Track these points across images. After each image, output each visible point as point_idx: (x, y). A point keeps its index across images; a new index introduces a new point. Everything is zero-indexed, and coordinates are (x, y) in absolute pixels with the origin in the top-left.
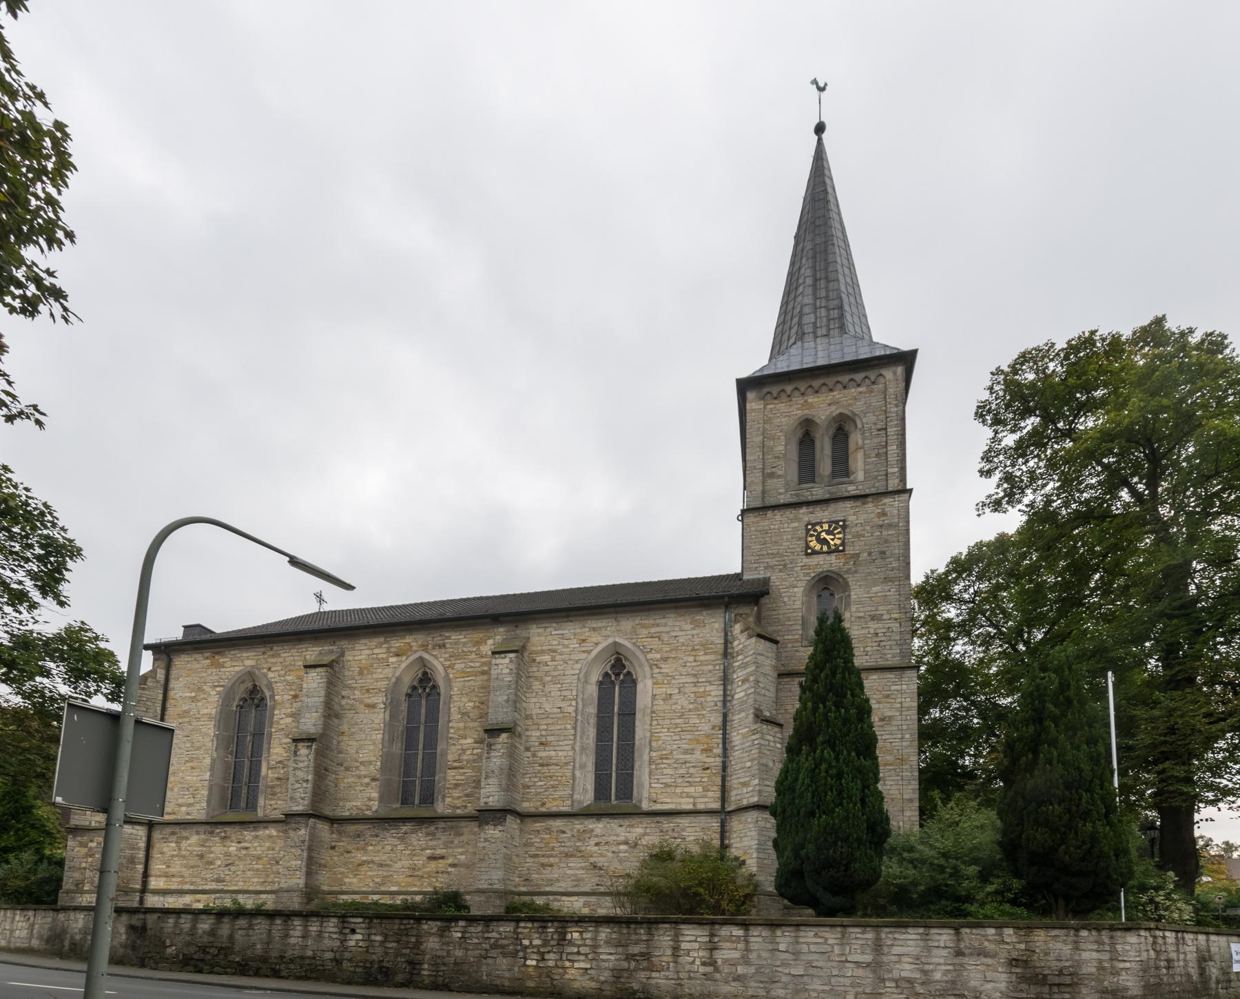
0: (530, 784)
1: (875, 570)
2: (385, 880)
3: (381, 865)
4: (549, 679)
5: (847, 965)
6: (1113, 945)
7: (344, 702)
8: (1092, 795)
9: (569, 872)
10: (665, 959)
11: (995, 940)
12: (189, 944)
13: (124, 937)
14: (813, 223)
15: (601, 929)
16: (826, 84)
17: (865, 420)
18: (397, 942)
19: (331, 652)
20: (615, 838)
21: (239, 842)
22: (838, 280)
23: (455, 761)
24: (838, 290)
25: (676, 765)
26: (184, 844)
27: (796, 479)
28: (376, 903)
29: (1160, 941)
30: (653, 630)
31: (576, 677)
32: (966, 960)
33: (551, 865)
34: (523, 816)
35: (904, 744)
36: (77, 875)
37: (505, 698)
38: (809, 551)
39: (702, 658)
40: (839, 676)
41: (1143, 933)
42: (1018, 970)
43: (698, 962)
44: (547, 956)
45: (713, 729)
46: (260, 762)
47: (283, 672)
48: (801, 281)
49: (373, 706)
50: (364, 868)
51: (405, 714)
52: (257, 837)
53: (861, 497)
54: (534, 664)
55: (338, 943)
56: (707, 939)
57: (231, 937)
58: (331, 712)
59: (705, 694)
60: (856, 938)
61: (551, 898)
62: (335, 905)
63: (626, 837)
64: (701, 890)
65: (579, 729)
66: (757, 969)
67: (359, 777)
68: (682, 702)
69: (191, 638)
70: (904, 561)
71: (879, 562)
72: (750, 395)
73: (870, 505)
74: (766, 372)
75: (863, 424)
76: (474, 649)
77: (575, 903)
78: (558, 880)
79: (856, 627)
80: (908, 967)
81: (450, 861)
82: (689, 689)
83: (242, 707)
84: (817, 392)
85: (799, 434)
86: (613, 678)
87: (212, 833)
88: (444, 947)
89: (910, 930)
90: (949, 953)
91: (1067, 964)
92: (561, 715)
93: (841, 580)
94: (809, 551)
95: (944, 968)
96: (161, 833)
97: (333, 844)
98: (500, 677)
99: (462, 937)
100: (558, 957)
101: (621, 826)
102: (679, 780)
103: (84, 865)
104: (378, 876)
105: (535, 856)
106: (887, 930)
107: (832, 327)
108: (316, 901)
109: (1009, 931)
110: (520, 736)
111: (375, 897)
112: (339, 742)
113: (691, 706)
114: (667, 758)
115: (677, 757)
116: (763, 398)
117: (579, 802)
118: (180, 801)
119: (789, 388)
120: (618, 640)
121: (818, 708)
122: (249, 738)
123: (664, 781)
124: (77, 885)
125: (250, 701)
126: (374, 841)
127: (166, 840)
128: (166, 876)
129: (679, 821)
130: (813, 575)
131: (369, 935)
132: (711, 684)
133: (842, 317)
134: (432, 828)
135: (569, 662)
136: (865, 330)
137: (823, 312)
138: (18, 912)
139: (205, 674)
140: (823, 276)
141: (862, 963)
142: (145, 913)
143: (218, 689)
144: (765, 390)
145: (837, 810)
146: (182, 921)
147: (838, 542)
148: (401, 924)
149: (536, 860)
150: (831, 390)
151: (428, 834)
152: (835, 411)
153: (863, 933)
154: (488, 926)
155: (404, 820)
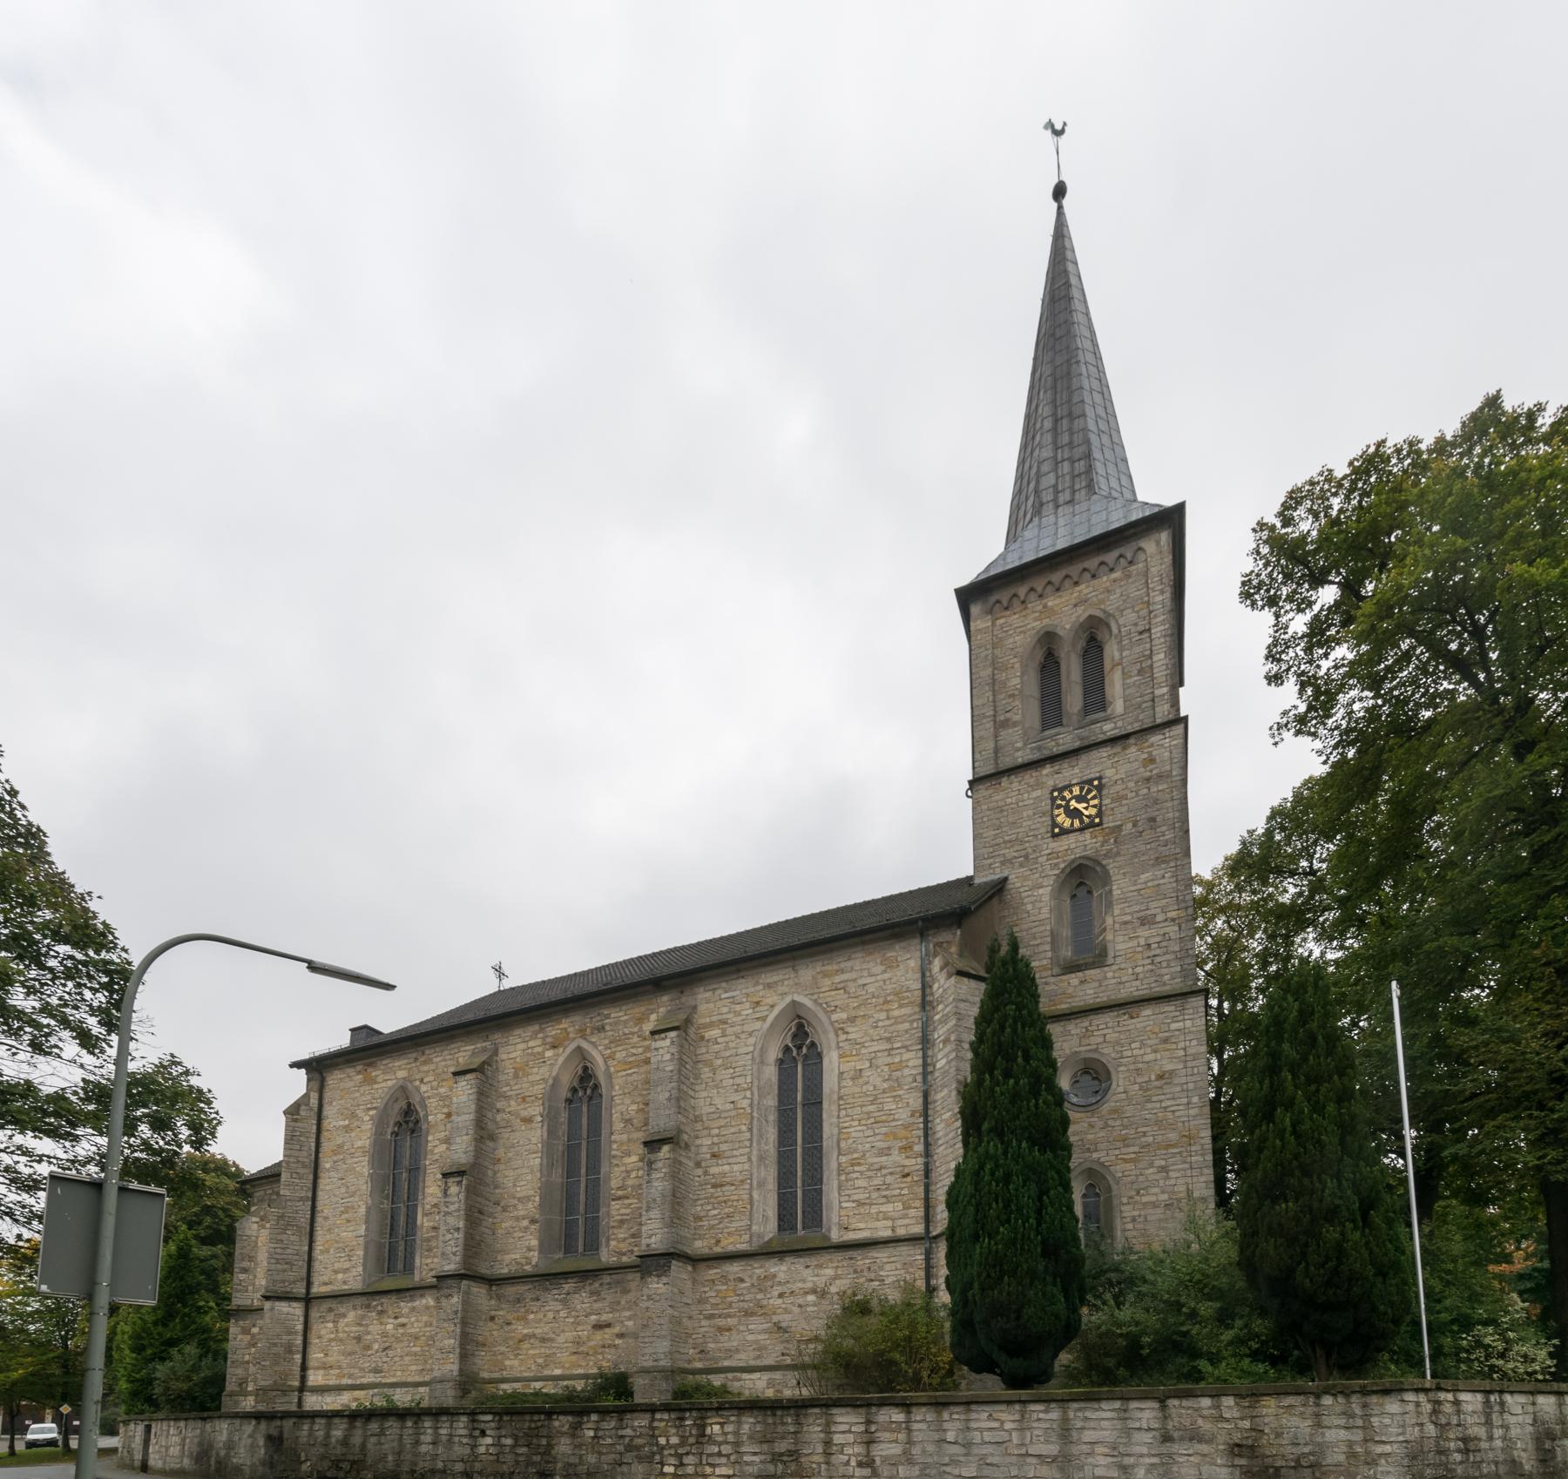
0: (702, 1214)
1: (1143, 848)
2: (549, 1359)
3: (543, 1340)
4: (719, 1062)
5: (1029, 1460)
6: (1366, 1417)
7: (499, 1117)
8: (1340, 1184)
9: (750, 1337)
10: (815, 1458)
11: (1211, 1416)
12: (323, 1457)
13: (263, 1451)
14: (1053, 335)
15: (744, 1419)
16: (1065, 124)
17: (1121, 621)
18: (527, 1446)
19: (484, 1050)
20: (800, 1285)
21: (396, 1318)
22: (1084, 415)
23: (618, 1188)
24: (1085, 430)
25: (869, 1174)
26: (342, 1323)
27: (1037, 723)
28: (537, 1394)
29: (1448, 1408)
30: (838, 979)
31: (750, 1056)
32: (1176, 1448)
33: (729, 1329)
34: (696, 1261)
35: (1192, 1112)
36: (240, 1371)
37: (667, 1095)
38: (1057, 830)
39: (896, 1013)
40: (1008, 1030)
41: (1410, 1397)
42: (1243, 1462)
43: (853, 1463)
44: (686, 1460)
45: (912, 1115)
46: (416, 1206)
47: (435, 1083)
48: (1038, 425)
49: (528, 1120)
50: (525, 1345)
51: (565, 1127)
52: (413, 1309)
53: (1123, 739)
54: (704, 1043)
55: (467, 1451)
56: (862, 1428)
57: (363, 1446)
58: (484, 1133)
59: (900, 1066)
60: (1039, 1420)
61: (730, 1375)
62: (494, 1397)
63: (814, 1282)
64: (897, 1356)
65: (755, 1131)
66: (921, 1470)
67: (517, 1219)
68: (874, 1079)
69: (362, 1044)
70: (1181, 828)
71: (1147, 835)
72: (975, 610)
73: (1133, 749)
74: (992, 573)
75: (1119, 627)
76: (636, 1030)
77: (758, 1383)
78: (737, 1351)
79: (1121, 939)
80: (1102, 1461)
81: (617, 1330)
82: (882, 1060)
83: (397, 1135)
84: (1058, 590)
85: (1039, 655)
86: (795, 1053)
87: (368, 1306)
88: (577, 1451)
89: (1104, 1405)
90: (1154, 1437)
91: (1306, 1450)
92: (733, 1113)
93: (1098, 869)
94: (1057, 830)
95: (1147, 1460)
96: (318, 1311)
97: (493, 1313)
98: (661, 1066)
99: (595, 1437)
100: (697, 1460)
101: (807, 1267)
102: (875, 1195)
103: (247, 1358)
104: (540, 1355)
105: (711, 1317)
106: (1075, 1405)
107: (1077, 487)
108: (474, 1394)
109: (1228, 1401)
110: (687, 1146)
111: (538, 1385)
112: (495, 1173)
113: (885, 1085)
114: (859, 1164)
115: (871, 1160)
116: (990, 612)
117: (759, 1236)
118: (337, 1266)
119: (1022, 591)
120: (797, 998)
121: (984, 1080)
122: (405, 1175)
123: (856, 1197)
124: (240, 1384)
125: (404, 1126)
126: (534, 1306)
127: (323, 1319)
128: (325, 1368)
129: (876, 1255)
130: (1062, 866)
131: (499, 1437)
132: (908, 1051)
133: (1090, 469)
134: (597, 1285)
135: (743, 1036)
136: (1124, 481)
137: (1066, 466)
138: (172, 1423)
139: (357, 1094)
140: (1065, 412)
141: (1047, 1457)
142: (282, 1418)
143: (372, 1113)
144: (993, 599)
145: (1001, 1229)
146: (316, 1427)
147: (1093, 811)
148: (532, 1421)
149: (714, 1322)
150: (1076, 583)
151: (592, 1293)
152: (1082, 613)
153: (1046, 1411)
154: (622, 1420)
155: (566, 1275)
